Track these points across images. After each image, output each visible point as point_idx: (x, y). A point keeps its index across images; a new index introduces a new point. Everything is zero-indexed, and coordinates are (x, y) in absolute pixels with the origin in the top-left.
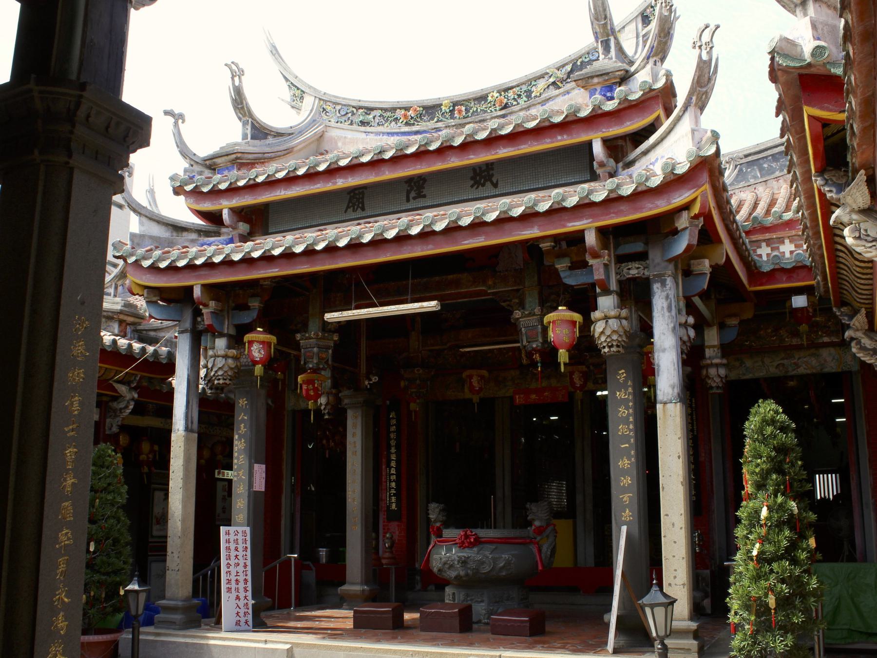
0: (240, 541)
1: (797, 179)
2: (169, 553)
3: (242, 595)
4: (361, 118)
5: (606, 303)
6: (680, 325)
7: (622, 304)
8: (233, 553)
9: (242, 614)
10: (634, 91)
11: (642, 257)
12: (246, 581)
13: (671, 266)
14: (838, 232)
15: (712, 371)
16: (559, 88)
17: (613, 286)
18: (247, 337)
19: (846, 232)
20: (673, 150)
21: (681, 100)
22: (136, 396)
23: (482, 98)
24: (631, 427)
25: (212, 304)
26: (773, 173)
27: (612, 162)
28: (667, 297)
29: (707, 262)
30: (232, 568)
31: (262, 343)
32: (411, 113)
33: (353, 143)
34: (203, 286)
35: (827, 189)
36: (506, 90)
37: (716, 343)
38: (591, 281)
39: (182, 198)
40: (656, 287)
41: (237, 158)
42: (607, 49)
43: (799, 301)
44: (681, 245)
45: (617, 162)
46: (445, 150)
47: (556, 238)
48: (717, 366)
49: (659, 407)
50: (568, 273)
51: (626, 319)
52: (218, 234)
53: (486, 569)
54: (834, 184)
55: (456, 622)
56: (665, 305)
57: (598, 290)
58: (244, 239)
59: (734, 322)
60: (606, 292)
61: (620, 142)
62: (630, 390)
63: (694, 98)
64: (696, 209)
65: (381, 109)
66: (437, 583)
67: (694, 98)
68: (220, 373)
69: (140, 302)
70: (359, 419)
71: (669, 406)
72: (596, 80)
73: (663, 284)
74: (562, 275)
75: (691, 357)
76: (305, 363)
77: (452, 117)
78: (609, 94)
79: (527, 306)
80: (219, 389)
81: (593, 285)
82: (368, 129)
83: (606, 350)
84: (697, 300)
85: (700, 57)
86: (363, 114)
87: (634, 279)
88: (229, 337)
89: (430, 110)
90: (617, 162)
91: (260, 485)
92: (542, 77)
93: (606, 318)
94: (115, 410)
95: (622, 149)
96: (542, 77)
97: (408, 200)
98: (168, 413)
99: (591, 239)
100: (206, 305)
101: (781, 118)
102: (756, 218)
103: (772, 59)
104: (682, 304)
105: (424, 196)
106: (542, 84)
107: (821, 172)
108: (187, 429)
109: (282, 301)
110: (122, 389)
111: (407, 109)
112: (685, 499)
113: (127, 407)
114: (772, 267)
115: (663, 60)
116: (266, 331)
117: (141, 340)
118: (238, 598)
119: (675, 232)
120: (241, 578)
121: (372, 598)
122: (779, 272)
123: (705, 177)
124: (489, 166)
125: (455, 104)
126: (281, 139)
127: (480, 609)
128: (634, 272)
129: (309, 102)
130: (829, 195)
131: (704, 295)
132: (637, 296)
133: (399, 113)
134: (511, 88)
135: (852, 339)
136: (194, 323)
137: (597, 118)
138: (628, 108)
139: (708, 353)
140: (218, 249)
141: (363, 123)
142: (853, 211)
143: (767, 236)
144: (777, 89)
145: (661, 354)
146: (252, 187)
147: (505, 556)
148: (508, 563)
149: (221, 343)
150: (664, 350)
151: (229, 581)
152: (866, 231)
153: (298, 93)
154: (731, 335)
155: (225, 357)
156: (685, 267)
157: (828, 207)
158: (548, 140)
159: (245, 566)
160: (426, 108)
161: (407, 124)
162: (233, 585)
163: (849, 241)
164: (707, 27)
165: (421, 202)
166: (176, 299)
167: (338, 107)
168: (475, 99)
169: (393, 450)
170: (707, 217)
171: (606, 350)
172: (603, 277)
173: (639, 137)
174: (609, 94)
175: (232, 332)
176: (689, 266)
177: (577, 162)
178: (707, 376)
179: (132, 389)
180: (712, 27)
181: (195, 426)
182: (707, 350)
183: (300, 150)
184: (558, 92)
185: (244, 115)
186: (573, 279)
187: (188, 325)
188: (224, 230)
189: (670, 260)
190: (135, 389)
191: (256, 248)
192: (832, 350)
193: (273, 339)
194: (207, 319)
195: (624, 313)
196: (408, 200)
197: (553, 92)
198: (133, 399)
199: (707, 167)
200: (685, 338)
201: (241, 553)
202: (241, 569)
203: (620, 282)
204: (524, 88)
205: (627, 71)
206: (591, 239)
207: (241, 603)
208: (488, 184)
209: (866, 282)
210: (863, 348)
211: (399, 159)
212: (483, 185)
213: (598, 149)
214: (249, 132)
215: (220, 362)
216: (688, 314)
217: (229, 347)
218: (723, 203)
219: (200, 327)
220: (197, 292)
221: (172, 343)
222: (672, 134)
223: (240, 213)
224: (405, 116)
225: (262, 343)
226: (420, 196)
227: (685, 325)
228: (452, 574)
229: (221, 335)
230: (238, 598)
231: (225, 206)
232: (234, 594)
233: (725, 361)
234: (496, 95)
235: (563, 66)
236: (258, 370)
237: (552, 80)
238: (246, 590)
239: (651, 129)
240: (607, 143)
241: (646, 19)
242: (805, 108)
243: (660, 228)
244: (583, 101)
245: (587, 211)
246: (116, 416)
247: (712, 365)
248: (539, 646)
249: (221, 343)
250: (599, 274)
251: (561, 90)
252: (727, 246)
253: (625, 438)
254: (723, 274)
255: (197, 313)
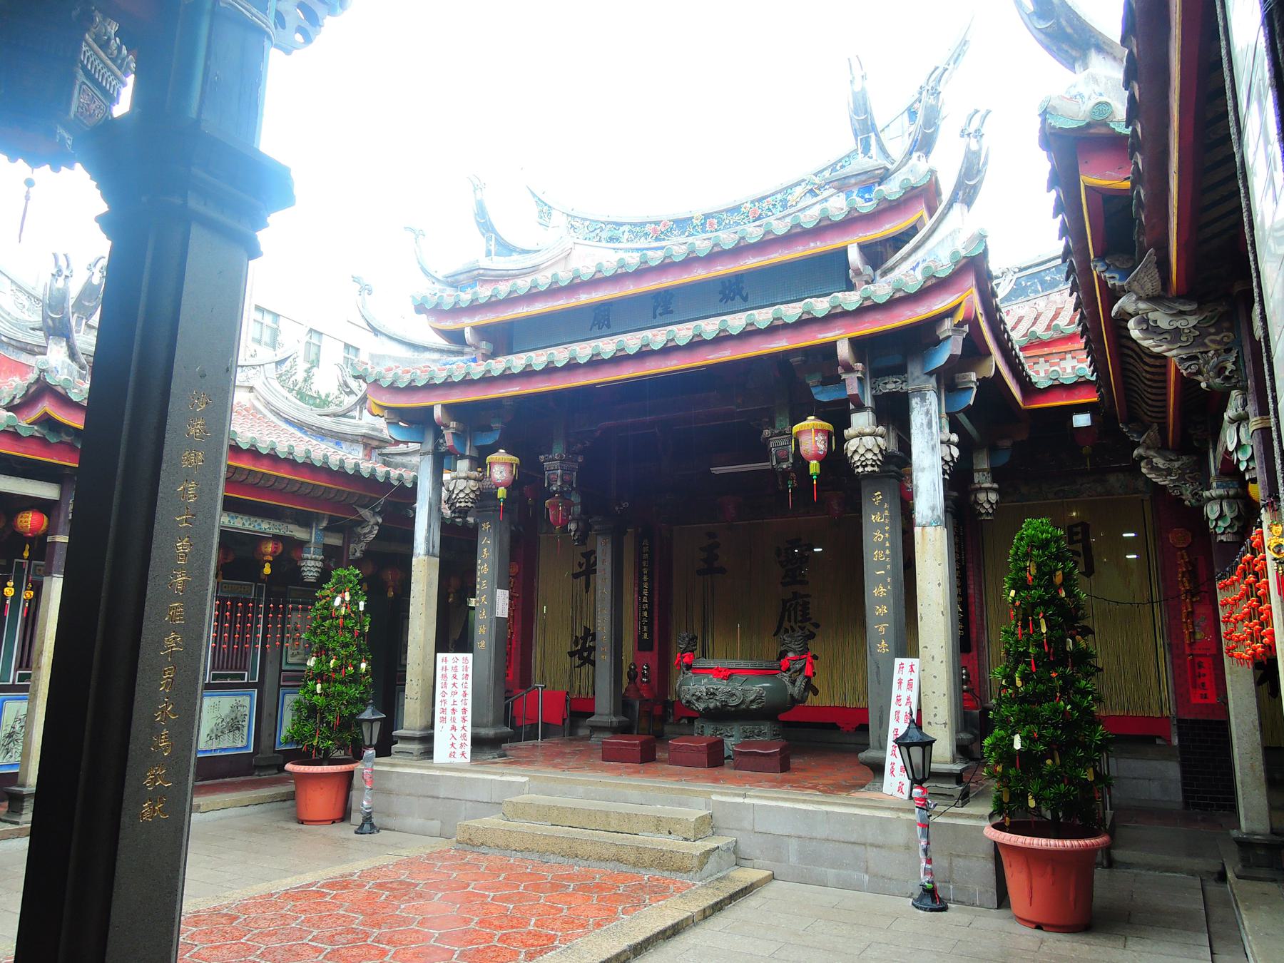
0: (460, 669)
1: (1074, 270)
2: (408, 680)
3: (459, 724)
4: (610, 234)
5: (862, 421)
6: (942, 442)
7: (879, 421)
8: (450, 681)
9: (457, 745)
10: (892, 189)
11: (900, 370)
12: (465, 710)
13: (933, 380)
14: (1123, 324)
15: (982, 497)
16: (817, 195)
17: (868, 402)
18: (489, 459)
19: (1131, 324)
20: (939, 249)
21: (946, 194)
22: (380, 520)
23: (736, 209)
24: (887, 552)
25: (453, 424)
26: (1057, 286)
27: (869, 270)
28: (927, 413)
29: (973, 376)
30: (447, 697)
31: (504, 464)
32: (661, 228)
33: (594, 258)
34: (444, 406)
35: (1107, 275)
36: (760, 200)
37: (986, 466)
38: (843, 397)
39: (424, 316)
40: (915, 402)
41: (479, 275)
42: (866, 149)
43: (1081, 420)
44: (941, 358)
45: (875, 269)
46: (691, 261)
47: (805, 351)
48: (987, 490)
49: (917, 530)
50: (820, 388)
51: (881, 436)
52: (461, 353)
53: (734, 702)
54: (1117, 269)
55: (704, 758)
56: (925, 422)
57: (852, 407)
58: (486, 357)
59: (1007, 443)
60: (860, 407)
61: (879, 249)
62: (887, 513)
63: (961, 193)
64: (960, 316)
65: (631, 224)
66: (688, 716)
67: (961, 193)
68: (462, 495)
69: (381, 423)
70: (609, 546)
71: (928, 529)
72: (853, 181)
73: (923, 399)
74: (814, 391)
75: (958, 481)
76: (550, 485)
77: (704, 231)
78: (867, 196)
79: (777, 425)
80: (464, 512)
81: (846, 402)
82: (617, 245)
83: (860, 470)
84: (963, 418)
85: (968, 146)
86: (610, 231)
87: (892, 395)
88: (471, 458)
89: (682, 224)
90: (875, 269)
91: (502, 610)
92: (798, 184)
93: (861, 435)
94: (359, 536)
95: (877, 255)
96: (798, 184)
97: (655, 317)
98: (409, 538)
99: (844, 351)
100: (447, 427)
101: (1060, 217)
102: (1034, 332)
103: (1044, 121)
104: (945, 422)
105: (671, 312)
106: (799, 191)
107: (1101, 256)
108: (428, 553)
109: (520, 423)
110: (366, 513)
111: (657, 223)
112: (946, 631)
113: (370, 532)
114: (1050, 383)
115: (927, 154)
116: (508, 452)
117: (386, 464)
118: (454, 728)
119: (938, 342)
120: (459, 707)
121: (623, 730)
122: (1058, 387)
123: (971, 281)
124: (738, 278)
125: (707, 216)
126: (526, 256)
127: (730, 744)
128: (891, 386)
129: (558, 219)
130: (1110, 283)
131: (968, 411)
132: (894, 413)
133: (649, 228)
134: (766, 197)
135: (1141, 458)
136: (437, 446)
137: (852, 221)
138: (890, 208)
139: (977, 477)
140: (459, 367)
141: (611, 239)
142: (1139, 299)
143: (1046, 350)
144: (1050, 158)
145: (920, 474)
146: (492, 305)
147: (757, 687)
148: (759, 697)
149: (463, 466)
150: (923, 470)
151: (443, 711)
152: (1155, 321)
153: (545, 211)
154: (1004, 458)
155: (467, 478)
156: (948, 381)
157: (1112, 295)
158: (800, 248)
159: (465, 694)
160: (675, 221)
161: (657, 239)
162: (449, 715)
163: (1135, 334)
164: (977, 112)
165: (668, 319)
166: (417, 420)
167: (587, 223)
168: (727, 211)
169: (645, 578)
170: (974, 324)
171: (860, 470)
172: (856, 392)
173: (898, 241)
174: (867, 196)
175: (475, 454)
176: (953, 379)
177: (832, 271)
178: (976, 502)
179: (375, 514)
180: (983, 112)
181: (437, 550)
182: (976, 475)
183: (545, 268)
184: (815, 200)
185: (488, 231)
186: (824, 395)
187: (429, 446)
188: (467, 350)
189: (930, 374)
190: (379, 513)
191: (498, 366)
192: (1121, 476)
193: (515, 460)
194: (449, 440)
195: (881, 429)
196: (655, 317)
197: (810, 200)
198: (377, 524)
199: (973, 266)
200: (948, 458)
201: (460, 681)
202: (459, 697)
203: (875, 398)
204: (779, 197)
205: (888, 170)
206: (844, 351)
207: (458, 734)
208: (738, 297)
209: (1156, 378)
210: (1154, 469)
211: (643, 272)
212: (733, 299)
213: (854, 256)
214: (493, 248)
215: (462, 484)
216: (951, 432)
217: (471, 469)
218: (992, 312)
219: (442, 449)
220: (438, 412)
221: (415, 468)
222: (936, 234)
223: (481, 331)
224: (655, 231)
225: (504, 464)
226: (668, 312)
227: (948, 443)
228: (701, 706)
229: (463, 457)
230: (454, 728)
231: (466, 324)
232: (449, 724)
233: (995, 486)
234: (748, 205)
235: (821, 172)
236: (502, 493)
237: (809, 187)
238: (464, 720)
239: (913, 231)
240: (864, 248)
241: (912, 114)
242: (1082, 178)
243: (920, 338)
244: (837, 205)
245: (839, 322)
246: (360, 541)
247: (981, 489)
248: (787, 786)
249: (463, 466)
250: (852, 388)
251: (819, 198)
252: (997, 358)
253: (881, 565)
254: (992, 386)
255: (438, 435)
